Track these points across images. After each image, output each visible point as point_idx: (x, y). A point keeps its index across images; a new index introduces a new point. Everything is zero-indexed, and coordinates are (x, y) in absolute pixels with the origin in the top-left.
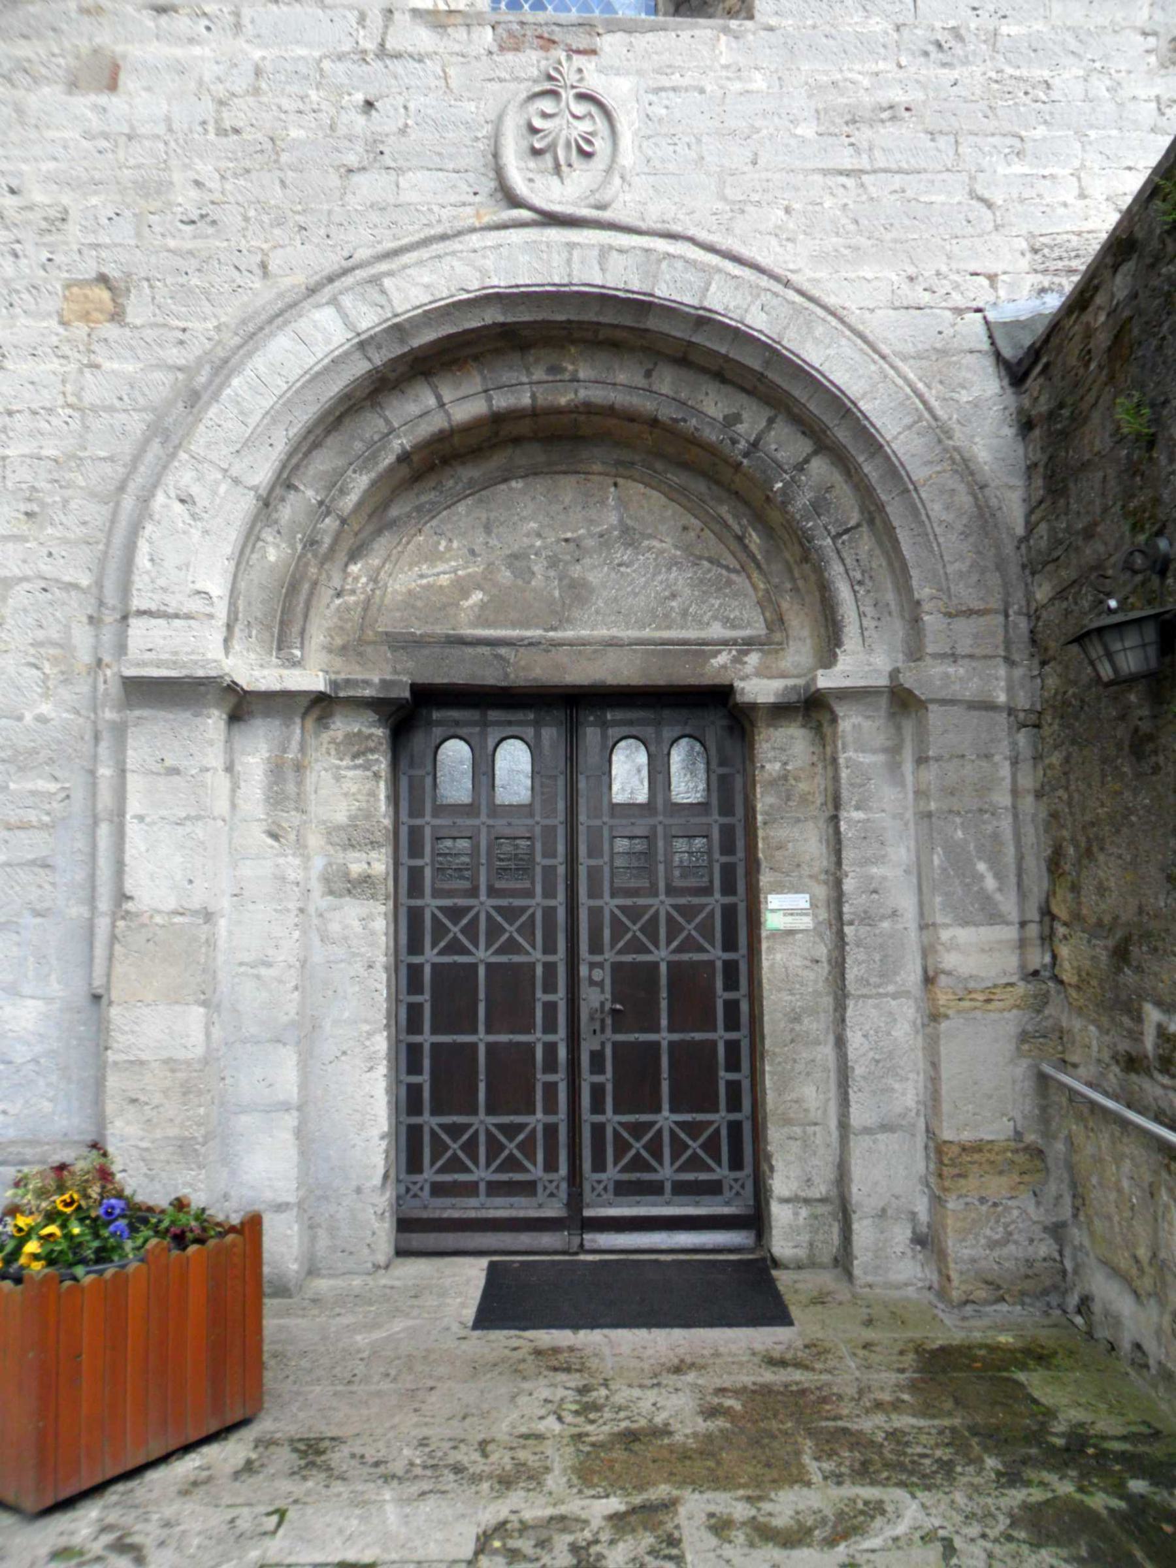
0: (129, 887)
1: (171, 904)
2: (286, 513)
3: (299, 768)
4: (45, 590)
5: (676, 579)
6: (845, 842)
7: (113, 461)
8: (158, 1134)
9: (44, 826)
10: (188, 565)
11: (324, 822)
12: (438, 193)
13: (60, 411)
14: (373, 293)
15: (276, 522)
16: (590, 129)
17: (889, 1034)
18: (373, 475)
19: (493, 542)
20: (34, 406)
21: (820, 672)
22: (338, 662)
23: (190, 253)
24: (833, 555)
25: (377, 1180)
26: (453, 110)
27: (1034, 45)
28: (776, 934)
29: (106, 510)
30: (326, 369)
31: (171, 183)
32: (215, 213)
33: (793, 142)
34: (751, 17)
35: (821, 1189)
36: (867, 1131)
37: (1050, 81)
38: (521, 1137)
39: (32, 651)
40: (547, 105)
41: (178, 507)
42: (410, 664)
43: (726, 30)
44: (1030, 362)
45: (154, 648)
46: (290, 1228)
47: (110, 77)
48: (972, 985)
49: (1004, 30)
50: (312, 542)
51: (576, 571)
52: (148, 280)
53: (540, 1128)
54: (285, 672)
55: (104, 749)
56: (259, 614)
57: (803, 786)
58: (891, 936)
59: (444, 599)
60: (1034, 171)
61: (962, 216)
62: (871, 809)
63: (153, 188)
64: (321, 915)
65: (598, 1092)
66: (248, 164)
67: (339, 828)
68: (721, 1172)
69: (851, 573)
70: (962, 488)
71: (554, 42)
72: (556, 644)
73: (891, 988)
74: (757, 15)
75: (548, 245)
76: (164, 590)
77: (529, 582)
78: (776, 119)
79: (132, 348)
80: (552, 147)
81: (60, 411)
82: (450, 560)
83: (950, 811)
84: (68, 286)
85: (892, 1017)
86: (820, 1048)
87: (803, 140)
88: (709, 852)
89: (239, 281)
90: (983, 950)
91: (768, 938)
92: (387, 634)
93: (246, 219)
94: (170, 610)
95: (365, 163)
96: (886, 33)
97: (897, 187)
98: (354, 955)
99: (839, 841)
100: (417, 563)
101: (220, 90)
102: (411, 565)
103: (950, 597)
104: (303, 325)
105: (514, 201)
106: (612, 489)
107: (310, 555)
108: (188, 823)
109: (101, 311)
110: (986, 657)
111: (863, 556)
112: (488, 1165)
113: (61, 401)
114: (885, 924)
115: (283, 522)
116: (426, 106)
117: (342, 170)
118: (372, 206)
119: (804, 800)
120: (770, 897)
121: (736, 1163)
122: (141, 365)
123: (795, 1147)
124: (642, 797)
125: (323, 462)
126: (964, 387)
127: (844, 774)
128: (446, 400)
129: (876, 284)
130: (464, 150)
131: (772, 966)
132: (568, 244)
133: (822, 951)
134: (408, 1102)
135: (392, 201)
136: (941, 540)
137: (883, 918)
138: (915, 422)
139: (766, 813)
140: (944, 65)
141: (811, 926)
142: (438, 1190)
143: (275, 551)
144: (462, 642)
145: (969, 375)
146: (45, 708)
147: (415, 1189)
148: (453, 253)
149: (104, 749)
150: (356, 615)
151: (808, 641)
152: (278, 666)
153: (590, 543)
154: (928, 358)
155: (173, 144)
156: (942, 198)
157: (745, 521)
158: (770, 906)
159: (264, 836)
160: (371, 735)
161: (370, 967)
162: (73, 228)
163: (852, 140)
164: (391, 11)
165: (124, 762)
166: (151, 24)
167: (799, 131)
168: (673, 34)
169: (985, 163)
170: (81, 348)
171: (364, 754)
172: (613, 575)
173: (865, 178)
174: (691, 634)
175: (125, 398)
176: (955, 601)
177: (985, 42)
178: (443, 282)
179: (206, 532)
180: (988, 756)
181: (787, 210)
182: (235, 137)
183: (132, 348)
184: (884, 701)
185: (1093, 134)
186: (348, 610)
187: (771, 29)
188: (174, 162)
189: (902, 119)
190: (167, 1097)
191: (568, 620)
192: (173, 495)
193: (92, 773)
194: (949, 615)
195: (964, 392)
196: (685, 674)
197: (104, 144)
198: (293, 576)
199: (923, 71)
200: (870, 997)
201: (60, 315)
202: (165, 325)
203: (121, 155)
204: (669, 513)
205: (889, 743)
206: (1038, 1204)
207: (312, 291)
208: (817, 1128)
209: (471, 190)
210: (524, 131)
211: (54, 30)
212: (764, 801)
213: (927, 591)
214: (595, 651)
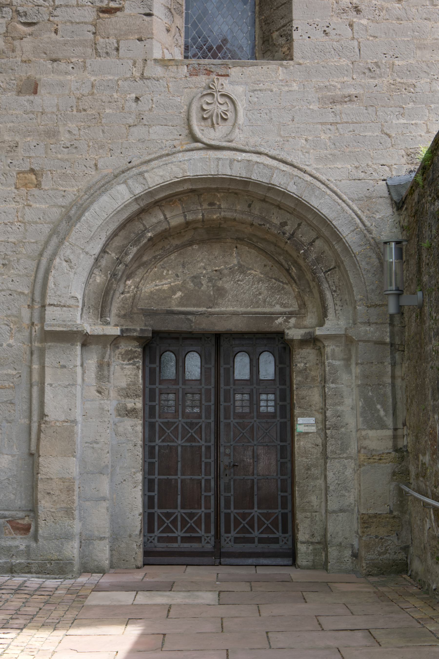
0: (46, 411)
1: (63, 418)
2: (103, 263)
3: (109, 365)
4: (11, 295)
5: (261, 287)
6: (327, 396)
7: (37, 243)
8: (58, 506)
9: (10, 388)
10: (69, 286)
11: (117, 387)
12: (165, 135)
13: (16, 223)
14: (141, 179)
15: (100, 266)
16: (226, 109)
17: (344, 473)
18: (138, 247)
19: (186, 271)
20: (6, 222)
21: (317, 328)
22: (122, 321)
23: (67, 160)
24: (324, 280)
25: (137, 532)
26: (171, 101)
27: (409, 69)
28: (300, 434)
29: (35, 263)
30: (122, 209)
31: (59, 132)
32: (76, 143)
33: (308, 111)
34: (292, 59)
35: (317, 539)
36: (334, 512)
37: (415, 84)
38: (195, 518)
39: (6, 319)
40: (209, 99)
41: (65, 264)
42: (152, 322)
43: (282, 65)
44: (407, 200)
45: (55, 319)
46: (106, 547)
47: (33, 88)
48: (374, 453)
49: (397, 63)
50: (114, 275)
51: (220, 284)
52: (50, 171)
53: (203, 515)
54: (105, 327)
55: (35, 357)
56: (93, 303)
57: (313, 373)
58: (345, 434)
59: (166, 295)
60: (408, 122)
61: (378, 141)
62: (338, 383)
63: (52, 134)
64: (115, 424)
65: (227, 500)
66: (89, 123)
67: (122, 389)
68: (279, 534)
69: (331, 287)
70: (374, 256)
71: (212, 72)
72: (211, 314)
73: (345, 455)
74: (294, 58)
75: (209, 159)
76: (60, 296)
77: (200, 288)
78: (302, 102)
79: (44, 199)
80: (211, 116)
81: (16, 223)
82: (168, 279)
83: (367, 385)
84: (18, 173)
85: (345, 467)
86: (318, 481)
87: (313, 110)
88: (201, 400)
89: (86, 172)
90: (378, 439)
91: (297, 435)
92: (142, 309)
93: (89, 146)
94: (62, 304)
95: (136, 123)
96: (348, 65)
97: (351, 129)
98: (129, 440)
99: (325, 396)
100: (154, 280)
101: (78, 94)
102: (152, 281)
103: (368, 300)
104: (113, 191)
105: (196, 140)
106: (235, 249)
107: (113, 280)
108: (69, 387)
109: (31, 183)
110: (382, 323)
111: (336, 280)
112: (181, 530)
113: (16, 220)
114: (343, 429)
115: (102, 266)
116: (160, 99)
117: (127, 126)
118: (139, 140)
119: (313, 379)
120: (298, 419)
121: (285, 531)
122: (48, 205)
123: (308, 521)
124: (247, 377)
125: (118, 242)
126: (378, 212)
127: (327, 369)
128: (168, 216)
129: (342, 170)
130: (175, 117)
131: (299, 447)
132: (217, 158)
133: (319, 441)
134: (149, 503)
135: (147, 139)
136: (365, 276)
137: (342, 427)
138: (355, 229)
139: (297, 384)
140: (372, 78)
141: (315, 431)
142: (160, 539)
143: (99, 279)
144: (173, 313)
145: (380, 207)
146: (11, 341)
147: (151, 539)
148: (172, 163)
149: (35, 357)
150: (130, 301)
151: (316, 313)
152: (101, 324)
153: (226, 272)
154: (363, 200)
155: (59, 116)
156: (370, 134)
157: (290, 263)
158: (299, 422)
159: (95, 392)
160: (136, 351)
161: (135, 445)
162: (20, 151)
163: (333, 110)
164: (146, 60)
165: (44, 363)
166: (50, 66)
167: (311, 107)
168: (260, 67)
169: (388, 119)
170: (24, 198)
171: (133, 359)
172: (235, 285)
173: (338, 126)
174: (267, 310)
175: (42, 218)
176: (370, 301)
177: (389, 68)
178: (168, 174)
179: (75, 273)
180: (382, 363)
181: (306, 140)
182: (84, 113)
183: (44, 199)
184: (343, 339)
185: (433, 106)
186: (126, 299)
187: (300, 64)
188: (60, 123)
189: (354, 101)
190: (61, 492)
191: (217, 304)
192: (63, 259)
193: (30, 367)
194: (368, 307)
195: (377, 214)
196: (264, 327)
197: (32, 116)
198: (107, 288)
199: (363, 81)
200: (336, 458)
201: (15, 184)
202: (57, 189)
203: (39, 120)
204: (259, 259)
205: (346, 357)
206: (398, 539)
207: (116, 177)
208: (317, 513)
209: (179, 134)
210: (200, 109)
211: (12, 69)
212: (297, 379)
213: (359, 297)
214: (228, 317)
